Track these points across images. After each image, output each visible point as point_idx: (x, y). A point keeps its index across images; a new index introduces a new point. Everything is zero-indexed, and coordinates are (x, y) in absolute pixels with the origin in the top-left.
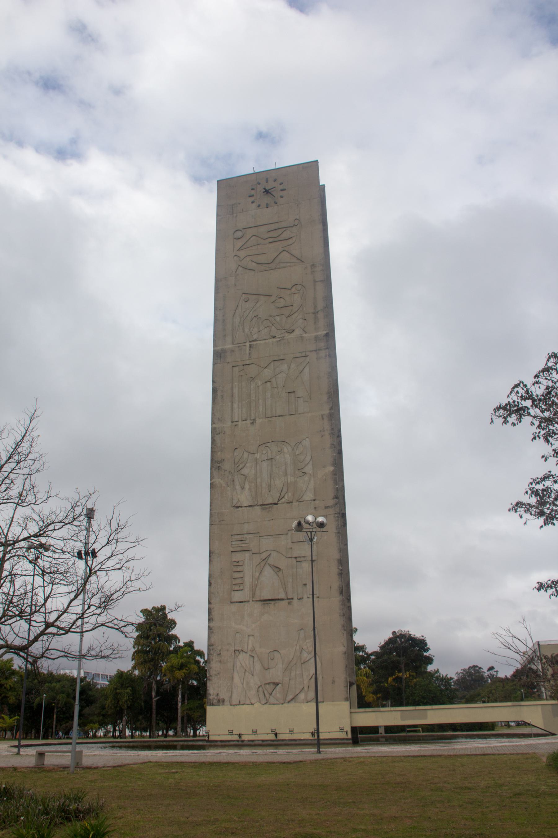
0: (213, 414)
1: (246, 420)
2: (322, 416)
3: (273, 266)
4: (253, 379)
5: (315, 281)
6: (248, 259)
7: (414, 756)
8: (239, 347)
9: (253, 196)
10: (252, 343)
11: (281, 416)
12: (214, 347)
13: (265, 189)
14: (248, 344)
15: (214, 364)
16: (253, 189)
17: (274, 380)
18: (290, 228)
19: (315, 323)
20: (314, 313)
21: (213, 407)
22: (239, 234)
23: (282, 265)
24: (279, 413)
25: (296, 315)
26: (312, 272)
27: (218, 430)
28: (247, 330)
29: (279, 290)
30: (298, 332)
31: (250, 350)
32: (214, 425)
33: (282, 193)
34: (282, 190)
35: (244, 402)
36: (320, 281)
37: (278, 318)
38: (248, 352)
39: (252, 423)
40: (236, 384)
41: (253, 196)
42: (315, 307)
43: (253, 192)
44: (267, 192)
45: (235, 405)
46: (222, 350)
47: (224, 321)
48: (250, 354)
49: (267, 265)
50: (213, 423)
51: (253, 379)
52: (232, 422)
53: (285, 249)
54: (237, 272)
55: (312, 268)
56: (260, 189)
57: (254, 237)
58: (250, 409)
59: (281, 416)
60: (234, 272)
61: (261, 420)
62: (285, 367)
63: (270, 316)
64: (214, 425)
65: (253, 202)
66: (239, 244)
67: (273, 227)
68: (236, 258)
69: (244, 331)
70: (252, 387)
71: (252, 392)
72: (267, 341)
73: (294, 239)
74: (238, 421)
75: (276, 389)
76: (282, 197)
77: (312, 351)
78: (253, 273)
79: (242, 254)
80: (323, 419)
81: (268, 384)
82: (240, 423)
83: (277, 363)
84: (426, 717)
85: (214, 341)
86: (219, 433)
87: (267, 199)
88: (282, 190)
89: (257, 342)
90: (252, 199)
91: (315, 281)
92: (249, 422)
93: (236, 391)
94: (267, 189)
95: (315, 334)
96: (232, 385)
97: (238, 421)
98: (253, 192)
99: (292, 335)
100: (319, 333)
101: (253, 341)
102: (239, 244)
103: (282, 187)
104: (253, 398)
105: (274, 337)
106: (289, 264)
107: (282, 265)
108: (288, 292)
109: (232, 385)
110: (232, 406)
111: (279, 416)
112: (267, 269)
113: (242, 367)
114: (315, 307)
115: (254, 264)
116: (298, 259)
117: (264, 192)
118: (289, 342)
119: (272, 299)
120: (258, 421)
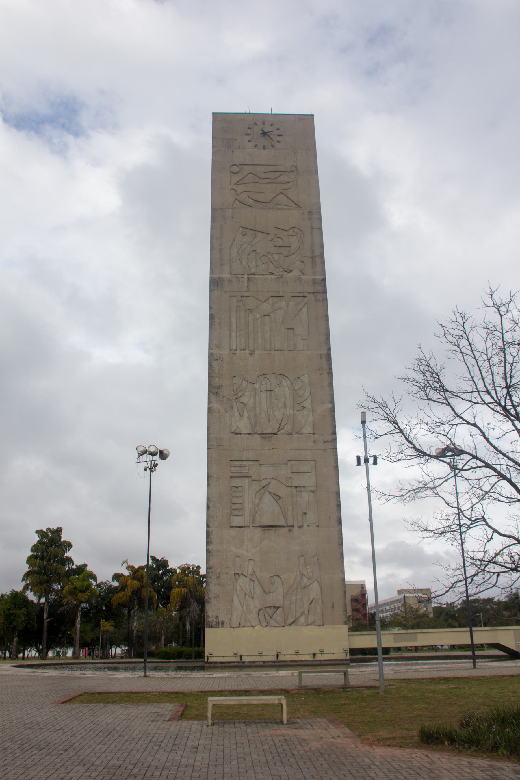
0: (210, 339)
1: (244, 350)
4: (251, 311)
5: (312, 228)
6: (245, 194)
8: (237, 278)
9: (250, 135)
10: (250, 276)
11: (280, 350)
12: (210, 274)
13: (262, 130)
14: (246, 276)
16: (250, 129)
17: (272, 315)
18: (287, 173)
20: (312, 258)
22: (236, 169)
23: (279, 207)
25: (293, 256)
26: (310, 219)
27: (215, 356)
28: (244, 263)
29: (277, 229)
30: (296, 273)
31: (248, 283)
33: (279, 138)
34: (279, 135)
35: (243, 332)
37: (276, 256)
38: (246, 284)
39: (251, 354)
41: (250, 135)
42: (313, 252)
43: (249, 131)
45: (233, 334)
46: (219, 278)
47: (221, 250)
49: (265, 204)
50: (210, 348)
51: (251, 311)
53: (283, 192)
54: (234, 205)
59: (280, 350)
60: (231, 205)
62: (283, 304)
63: (269, 253)
64: (211, 351)
65: (249, 141)
66: (236, 178)
67: (270, 169)
68: (232, 191)
69: (241, 263)
70: (250, 318)
71: (250, 324)
74: (236, 350)
76: (279, 142)
77: (310, 293)
78: (250, 209)
79: (240, 188)
80: (321, 358)
81: (267, 318)
82: (238, 352)
83: (276, 299)
86: (217, 359)
88: (279, 135)
90: (249, 138)
91: (312, 228)
92: (247, 352)
93: (234, 320)
94: (266, 131)
95: (313, 277)
97: (236, 350)
98: (249, 131)
99: (290, 275)
100: (317, 277)
101: (251, 274)
102: (236, 178)
103: (278, 132)
104: (251, 329)
105: (273, 274)
107: (279, 207)
110: (230, 334)
111: (278, 350)
113: (240, 298)
114: (313, 252)
115: (251, 200)
116: (295, 204)
117: (261, 134)
118: (287, 281)
120: (257, 352)
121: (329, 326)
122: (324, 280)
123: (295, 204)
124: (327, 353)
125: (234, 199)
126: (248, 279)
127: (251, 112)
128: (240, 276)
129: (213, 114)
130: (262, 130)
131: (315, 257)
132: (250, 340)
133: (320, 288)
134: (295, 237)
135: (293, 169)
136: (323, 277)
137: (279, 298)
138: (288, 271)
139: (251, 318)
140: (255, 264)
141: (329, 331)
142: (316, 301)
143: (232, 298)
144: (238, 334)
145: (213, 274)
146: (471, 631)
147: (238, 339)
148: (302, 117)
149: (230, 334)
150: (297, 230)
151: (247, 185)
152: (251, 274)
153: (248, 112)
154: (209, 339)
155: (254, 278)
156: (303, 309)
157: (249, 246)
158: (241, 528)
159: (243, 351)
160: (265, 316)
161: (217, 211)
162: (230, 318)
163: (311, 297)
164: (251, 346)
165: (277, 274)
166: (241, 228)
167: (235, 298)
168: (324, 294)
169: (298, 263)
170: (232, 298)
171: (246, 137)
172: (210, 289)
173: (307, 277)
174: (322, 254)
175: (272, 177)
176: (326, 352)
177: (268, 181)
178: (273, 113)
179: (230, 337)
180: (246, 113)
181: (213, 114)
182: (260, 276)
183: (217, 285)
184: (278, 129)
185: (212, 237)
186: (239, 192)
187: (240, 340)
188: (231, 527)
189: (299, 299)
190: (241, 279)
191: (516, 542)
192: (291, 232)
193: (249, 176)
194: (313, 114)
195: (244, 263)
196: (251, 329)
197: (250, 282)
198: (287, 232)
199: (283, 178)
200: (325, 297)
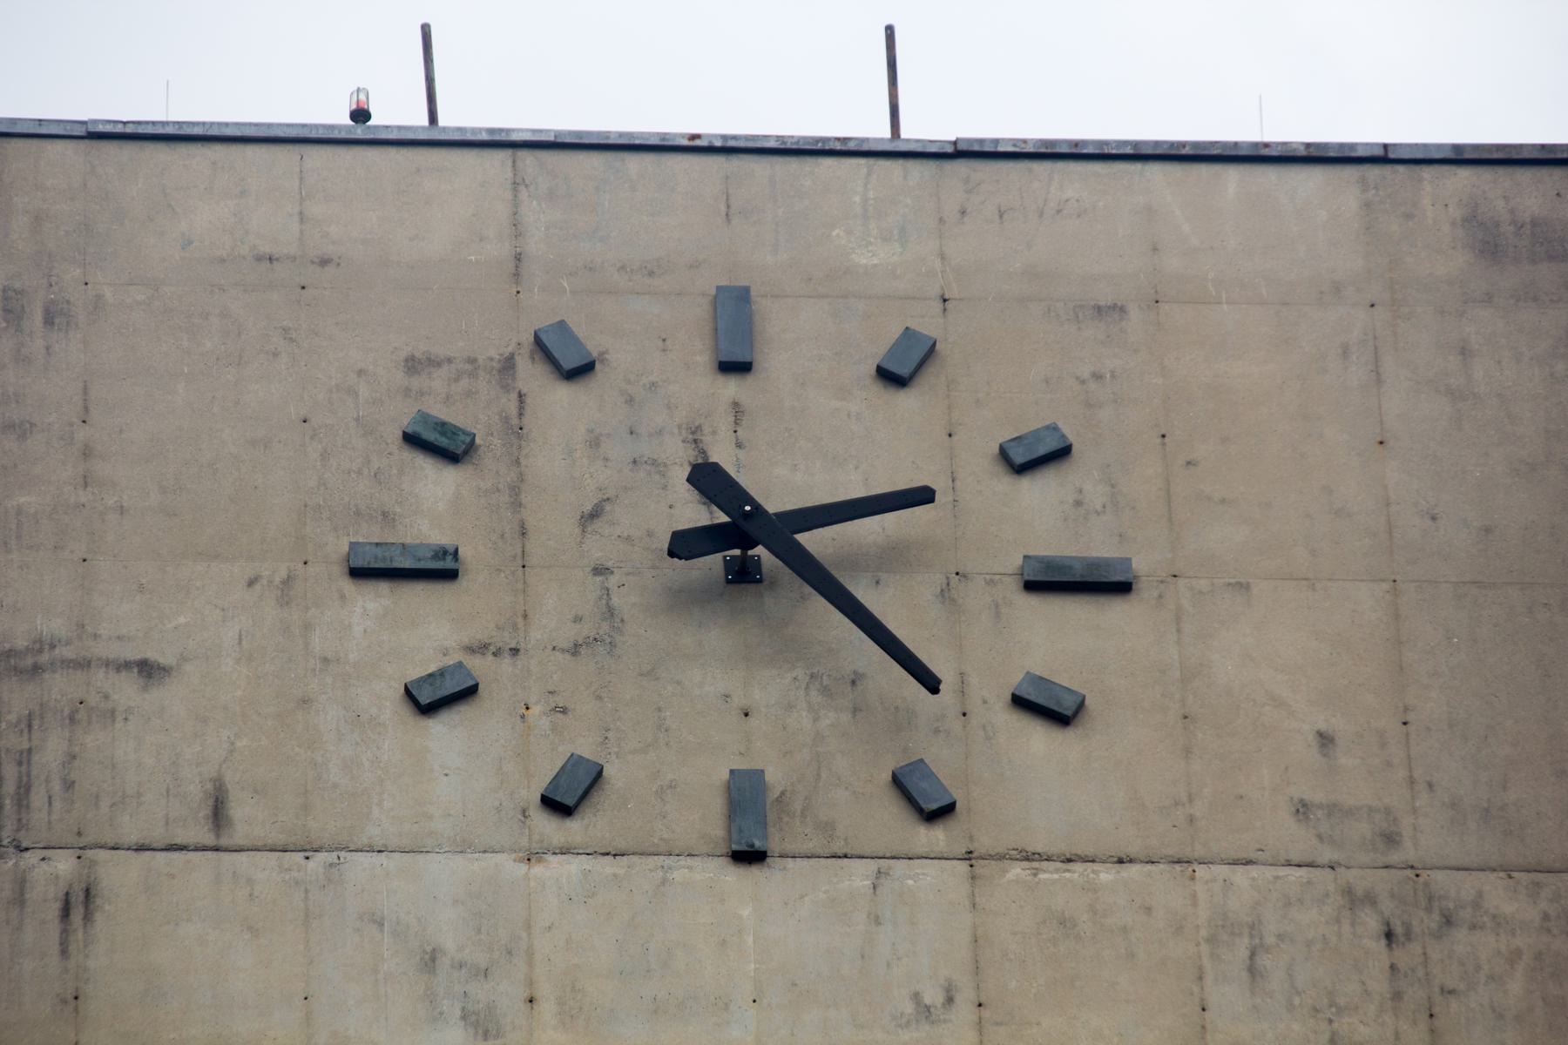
9: (440, 570)
13: (709, 480)
16: (440, 445)
33: (1058, 641)
34: (1050, 582)
41: (440, 570)
43: (433, 505)
44: (743, 543)
65: (436, 698)
76: (1049, 709)
84: (586, 873)
87: (726, 699)
88: (1050, 582)
90: (428, 631)
94: (778, 487)
103: (1042, 518)
117: (684, 545)
127: (462, 112)
130: (709, 480)
146: (433, 118)
153: (399, 110)
158: (175, 855)
171: (375, 599)
180: (360, 134)
184: (1036, 458)
191: (810, 540)
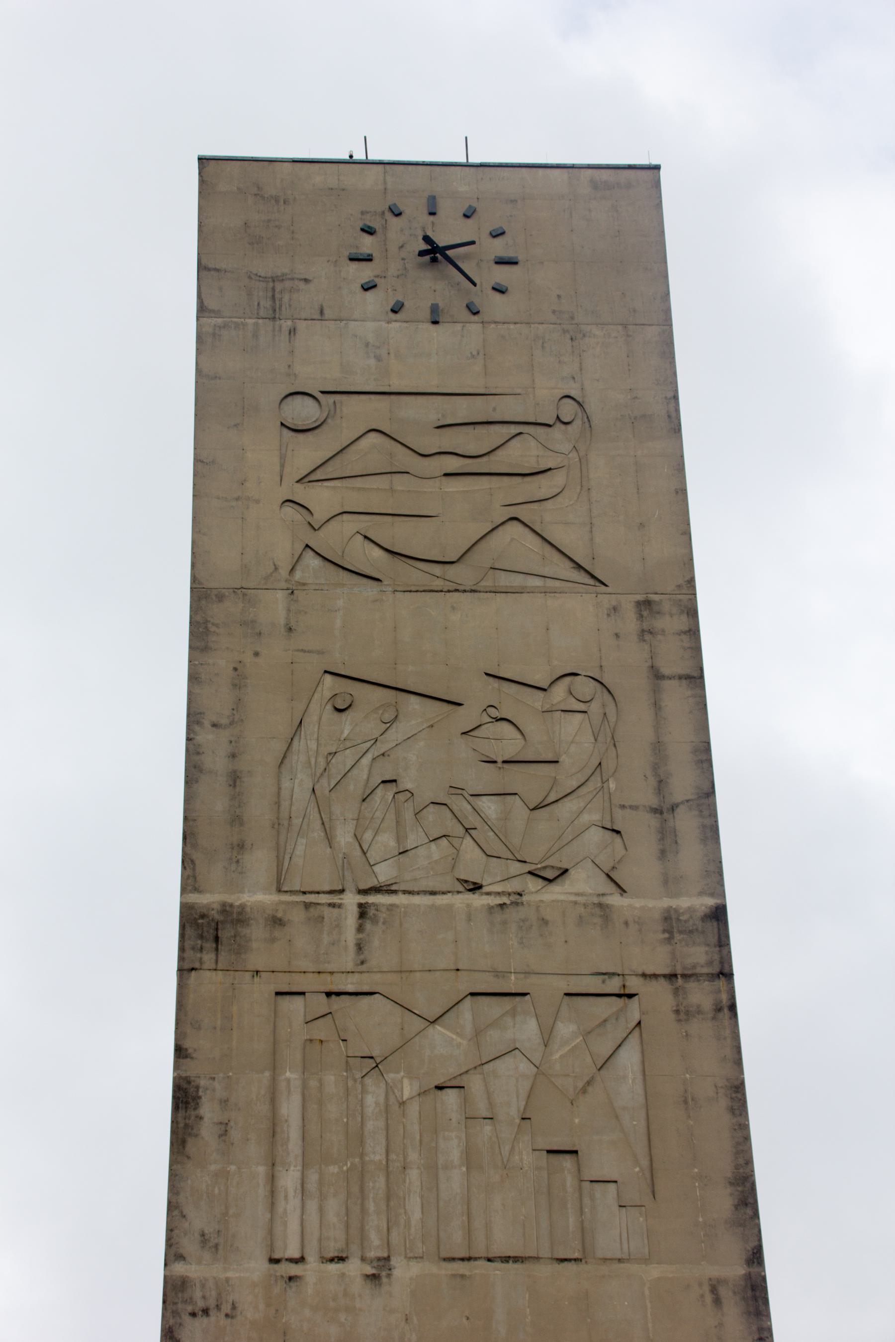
0: (175, 1208)
1: (341, 1259)
2: (714, 1290)
3: (461, 574)
4: (375, 1064)
5: (657, 675)
6: (350, 525)
7: (295, 161)
8: (307, 906)
9: (369, 259)
10: (371, 899)
11: (516, 1259)
12: (184, 890)
13: (427, 239)
14: (351, 900)
15: (185, 971)
16: (369, 231)
17: (475, 1083)
18: (541, 430)
19: (663, 853)
20: (657, 811)
21: (174, 1176)
22: (303, 411)
23: (505, 580)
24: (502, 1244)
25: (569, 806)
26: (646, 634)
27: (198, 1294)
28: (344, 837)
29: (495, 683)
30: (583, 883)
31: (360, 929)
32: (180, 1268)
33: (502, 275)
34: (500, 262)
35: (334, 1169)
36: (680, 677)
37: (490, 807)
38: (350, 935)
39: (374, 1278)
40: (291, 1076)
41: (369, 259)
42: (661, 784)
43: (367, 244)
44: (434, 253)
45: (289, 1179)
46: (226, 909)
47: (235, 779)
48: (359, 947)
49: (437, 569)
50: (174, 1253)
51: (375, 1064)
52: (274, 1261)
53: (522, 512)
54: (298, 575)
55: (641, 617)
56: (404, 237)
57: (373, 438)
58: (364, 1211)
59: (516, 1259)
60: (284, 572)
61: (415, 1269)
62: (527, 1030)
63: (456, 790)
64: (180, 1268)
66: (307, 453)
67: (463, 410)
68: (289, 510)
69: (329, 839)
70: (370, 1100)
71: (370, 1125)
72: (440, 900)
73: (557, 480)
74: (301, 1260)
75: (488, 1128)
76: (500, 290)
77: (655, 976)
78: (370, 590)
79: (322, 499)
80: (717, 1301)
81: (451, 1097)
82: (311, 1270)
83: (494, 1008)
85: (187, 861)
86: (206, 1312)
87: (430, 287)
88: (500, 262)
89: (399, 899)
90: (366, 272)
91: (657, 675)
92: (354, 1268)
93: (291, 1108)
94: (442, 241)
95: (666, 902)
96: (274, 1079)
97: (301, 1260)
98: (367, 244)
99: (556, 893)
100: (684, 903)
101: (377, 890)
102: (307, 453)
103: (499, 248)
104: (376, 1153)
105: (476, 888)
106: (538, 582)
107: (505, 580)
108: (537, 700)
109: (274, 1079)
110: (272, 1179)
111: (506, 1259)
112: (438, 584)
113: (321, 1004)
114: (661, 784)
115: (377, 553)
116: (579, 567)
117: (422, 253)
118: (545, 922)
119: (466, 717)
120: (404, 1271)
121: (747, 1139)
122: (719, 915)
123: (579, 567)
124: (748, 1277)
125: (300, 547)
126: (363, 911)
128: (324, 899)
129: (216, 175)
130: (427, 239)
131: (673, 808)
132: (371, 1207)
133: (698, 955)
134: (579, 716)
135: (568, 410)
136: (711, 902)
137: (508, 1003)
138: (550, 874)
139: (374, 1098)
140: (392, 843)
141: (749, 1162)
142: (683, 1014)
143: (286, 1003)
144: (313, 1177)
145: (196, 890)
147: (312, 1206)
148: (604, 175)
149: (272, 1179)
150: (584, 687)
151: (359, 483)
152: (377, 890)
153: (359, 156)
154: (172, 1207)
155: (391, 907)
156: (623, 1053)
157: (366, 761)
159: (333, 1267)
160: (440, 1088)
161: (221, 598)
162: (273, 1100)
163: (659, 996)
164: (374, 1239)
165: (498, 888)
166: (328, 677)
167: (299, 1000)
168: (722, 983)
169: (595, 836)
170: (285, 1001)
171: (355, 265)
172: (181, 959)
173: (638, 903)
174: (708, 793)
175: (473, 450)
176: (741, 1270)
177: (454, 464)
178: (474, 159)
179: (273, 1193)
180: (351, 161)
181: (216, 175)
182: (416, 900)
183: (217, 939)
185: (194, 718)
186: (320, 515)
187: (321, 1210)
188: (616, 1182)
189: (604, 1008)
190: (327, 912)
192: (559, 692)
193: (365, 443)
194: (654, 162)
195: (344, 837)
196: (376, 1153)
197: (368, 926)
198: (541, 694)
199: (523, 453)
200: (724, 997)
